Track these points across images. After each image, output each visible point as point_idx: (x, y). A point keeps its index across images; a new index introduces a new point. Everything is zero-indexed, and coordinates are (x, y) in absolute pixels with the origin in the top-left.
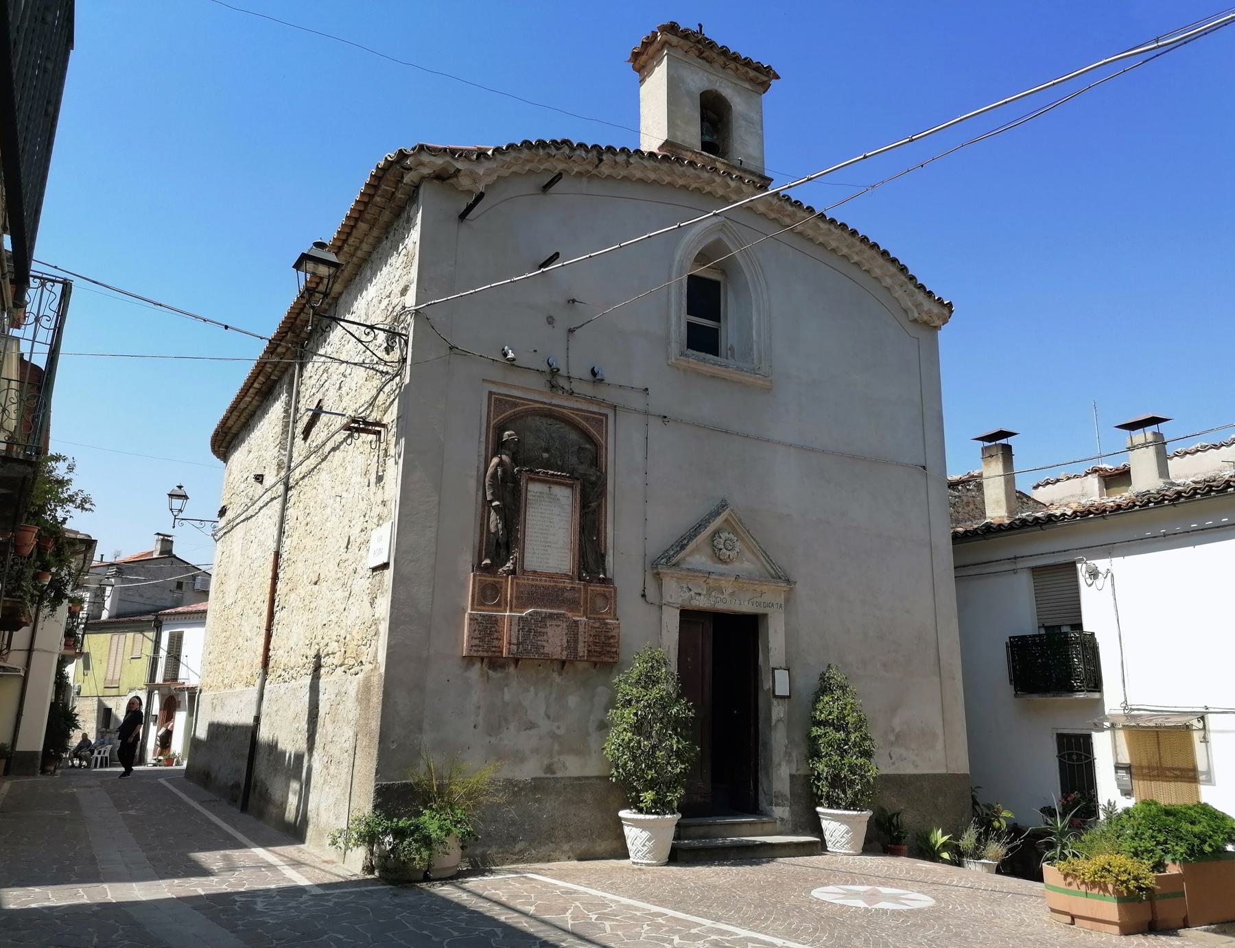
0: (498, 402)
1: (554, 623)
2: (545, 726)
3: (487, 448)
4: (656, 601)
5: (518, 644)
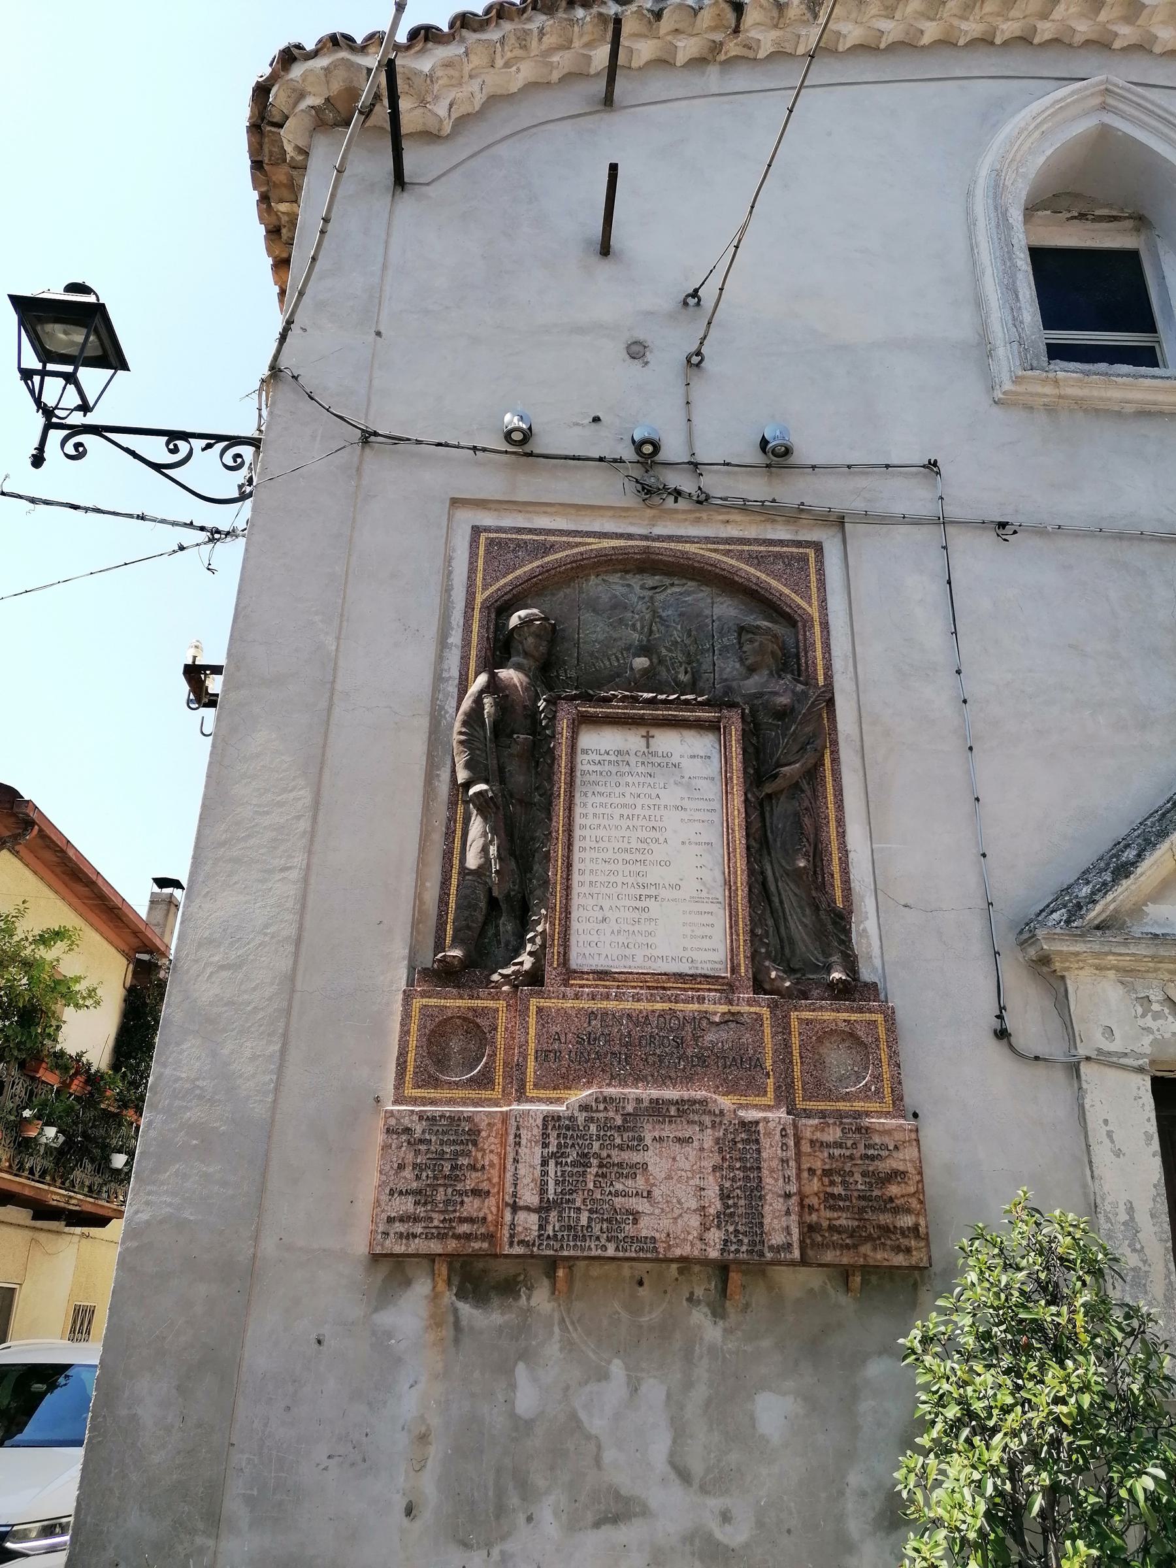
0: (496, 548)
1: (668, 1131)
2: (673, 1510)
3: (465, 658)
4: (1056, 1050)
5: (543, 1209)
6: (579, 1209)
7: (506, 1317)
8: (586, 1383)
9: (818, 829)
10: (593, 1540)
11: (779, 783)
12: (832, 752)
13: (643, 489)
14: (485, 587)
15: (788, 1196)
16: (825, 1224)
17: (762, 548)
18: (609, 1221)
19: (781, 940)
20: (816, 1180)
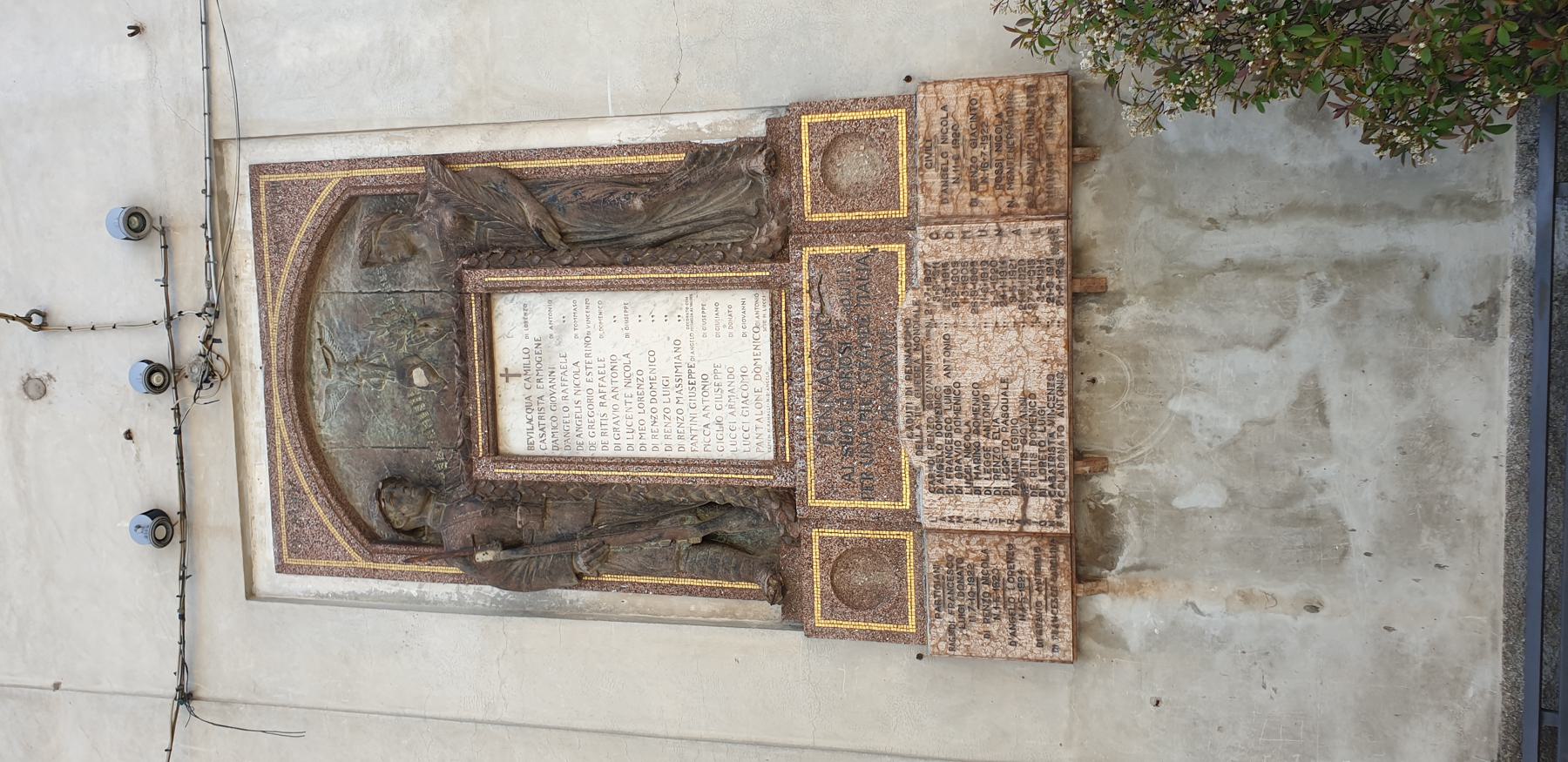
0: (297, 551)
1: (938, 361)
5: (1024, 492)
6: (1022, 455)
7: (1131, 519)
8: (1192, 436)
9: (596, 179)
10: (1339, 428)
11: (546, 225)
12: (505, 159)
13: (207, 381)
14: (349, 558)
15: (1000, 232)
16: (1027, 189)
17: (265, 237)
18: (1033, 423)
19: (726, 223)
20: (981, 199)
